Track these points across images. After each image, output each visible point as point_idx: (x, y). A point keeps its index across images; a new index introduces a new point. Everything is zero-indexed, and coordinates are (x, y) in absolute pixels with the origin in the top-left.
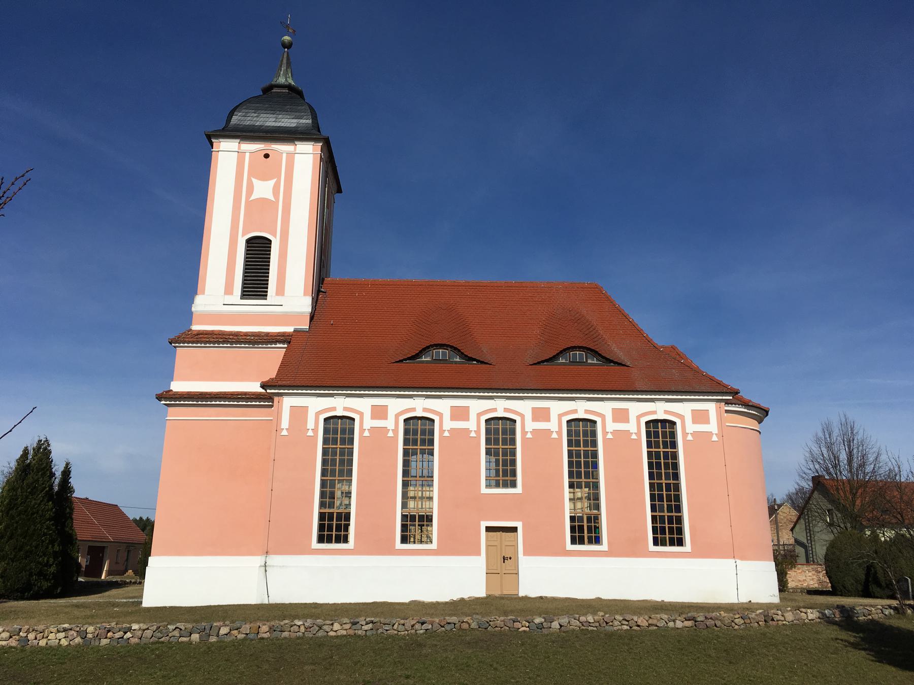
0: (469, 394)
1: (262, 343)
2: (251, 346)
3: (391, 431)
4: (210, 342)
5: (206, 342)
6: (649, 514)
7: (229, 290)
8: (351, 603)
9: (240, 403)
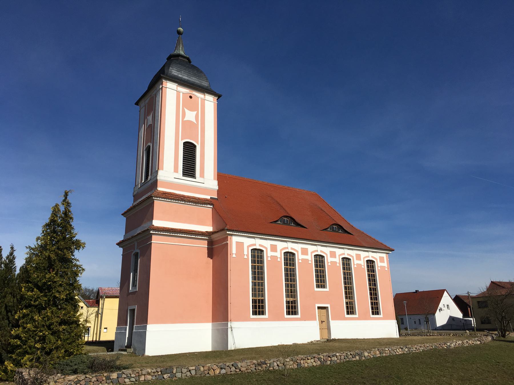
0: (239, 234)
1: (200, 203)
2: (195, 204)
3: (269, 257)
4: (174, 199)
5: (171, 199)
7: (176, 170)
8: (365, 339)
9: (192, 236)
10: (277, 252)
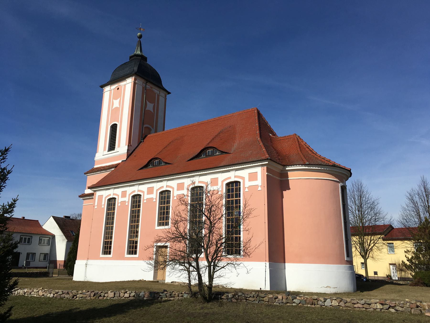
6: (113, 240)
7: (105, 150)
10: (177, 191)
